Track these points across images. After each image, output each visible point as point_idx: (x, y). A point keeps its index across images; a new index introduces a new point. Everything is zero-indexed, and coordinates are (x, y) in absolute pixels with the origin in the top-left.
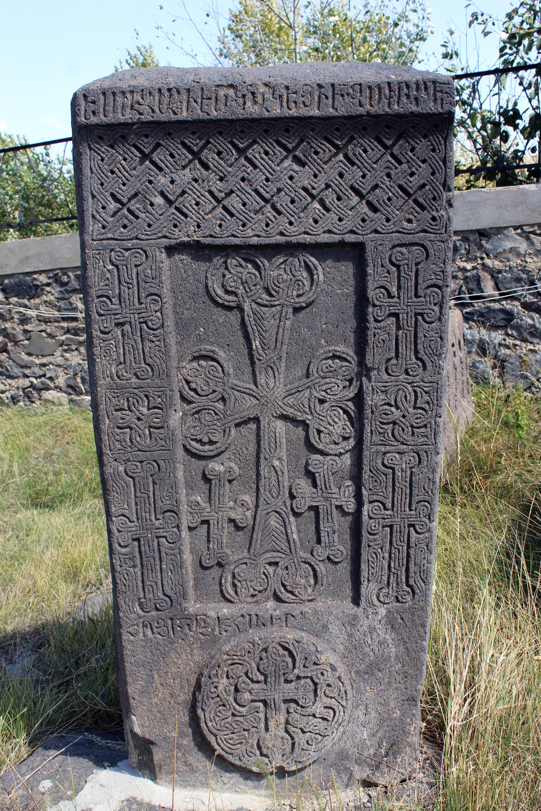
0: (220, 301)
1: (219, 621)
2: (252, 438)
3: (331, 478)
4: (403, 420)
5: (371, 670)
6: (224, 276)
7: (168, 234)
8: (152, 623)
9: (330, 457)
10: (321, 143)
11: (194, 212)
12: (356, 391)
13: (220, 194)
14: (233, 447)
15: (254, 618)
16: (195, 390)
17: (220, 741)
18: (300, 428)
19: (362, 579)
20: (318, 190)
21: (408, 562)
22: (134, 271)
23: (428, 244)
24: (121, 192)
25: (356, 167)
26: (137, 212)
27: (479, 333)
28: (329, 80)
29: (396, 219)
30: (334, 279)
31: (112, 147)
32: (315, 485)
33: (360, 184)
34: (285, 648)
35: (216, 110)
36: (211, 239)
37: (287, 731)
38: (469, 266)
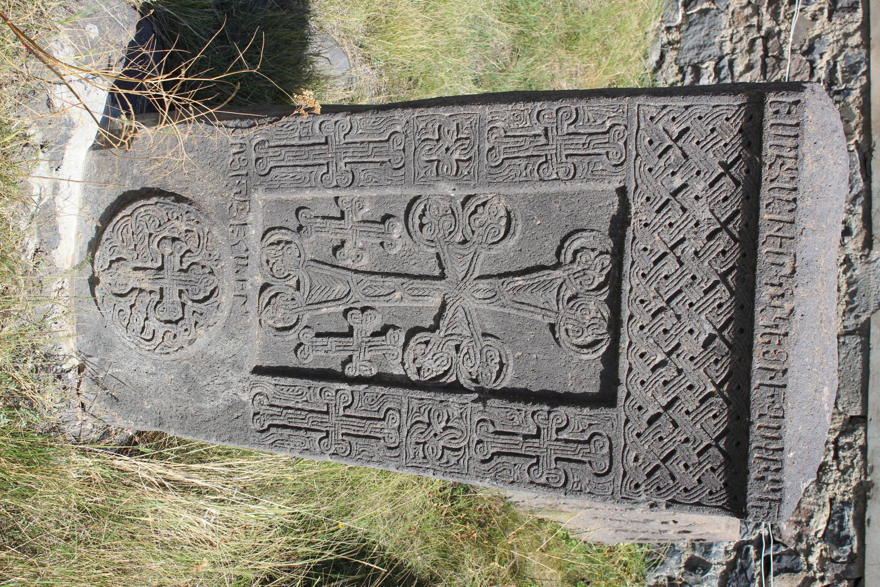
0: (566, 245)
1: (243, 225)
2: (425, 271)
3: (380, 353)
4: (432, 434)
5: (189, 382)
6: (593, 250)
7: (639, 190)
8: (244, 154)
9: (401, 354)
10: (726, 368)
11: (662, 220)
12: (465, 386)
13: (680, 251)
14: (417, 249)
15: (244, 262)
16: (475, 212)
17: (126, 219)
18: (432, 323)
19: (278, 378)
20: (676, 361)
21: (292, 428)
22: (603, 151)
23: (610, 477)
24: (690, 139)
25: (698, 404)
26: (665, 157)
27: (718, 563)
28: (791, 383)
29: (639, 443)
31: (740, 131)
32: (374, 334)
33: (680, 408)
34: (212, 292)
35: (767, 252)
36: (631, 238)
37: (133, 289)
38: (813, 559)
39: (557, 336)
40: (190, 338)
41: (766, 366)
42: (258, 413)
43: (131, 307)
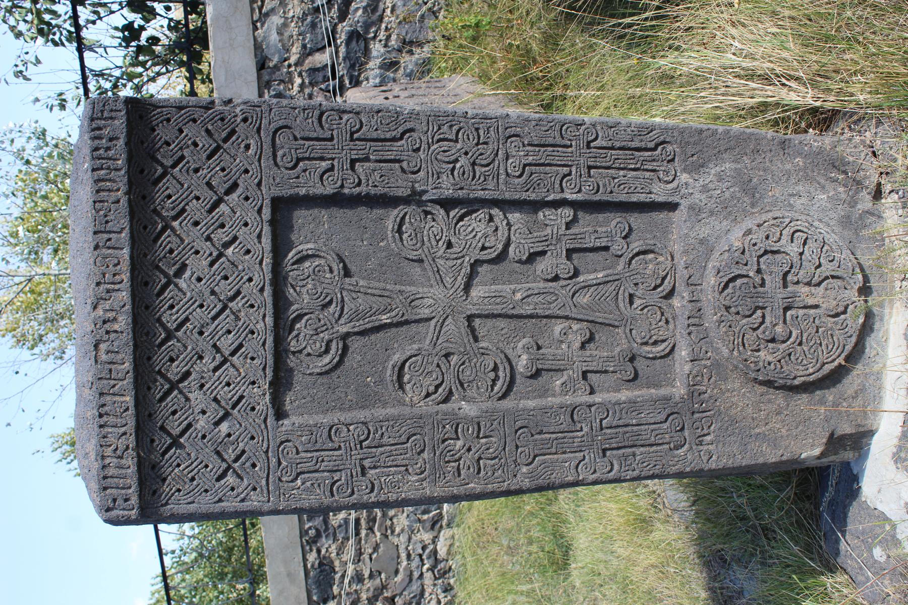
0: (337, 359)
2: (490, 323)
3: (535, 234)
4: (470, 154)
5: (751, 191)
6: (309, 355)
8: (698, 435)
9: (512, 235)
10: (161, 246)
12: (438, 207)
13: (217, 359)
14: (501, 345)
15: (692, 321)
16: (437, 387)
17: (830, 359)
18: (480, 269)
19: (648, 200)
20: (212, 249)
21: (629, 149)
22: (303, 455)
23: (273, 126)
24: (214, 470)
26: (238, 452)
28: (90, 237)
29: (245, 162)
30: (312, 231)
31: (164, 480)
32: (543, 253)
33: (206, 202)
34: (726, 286)
35: (124, 364)
38: (298, 81)
39: (341, 265)
40: (750, 236)
41: (116, 251)
42: (669, 161)
43: (820, 266)
